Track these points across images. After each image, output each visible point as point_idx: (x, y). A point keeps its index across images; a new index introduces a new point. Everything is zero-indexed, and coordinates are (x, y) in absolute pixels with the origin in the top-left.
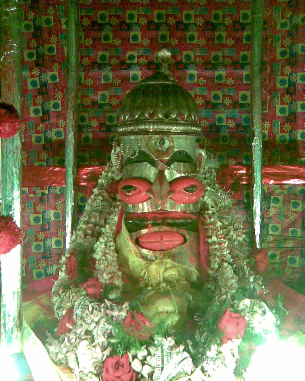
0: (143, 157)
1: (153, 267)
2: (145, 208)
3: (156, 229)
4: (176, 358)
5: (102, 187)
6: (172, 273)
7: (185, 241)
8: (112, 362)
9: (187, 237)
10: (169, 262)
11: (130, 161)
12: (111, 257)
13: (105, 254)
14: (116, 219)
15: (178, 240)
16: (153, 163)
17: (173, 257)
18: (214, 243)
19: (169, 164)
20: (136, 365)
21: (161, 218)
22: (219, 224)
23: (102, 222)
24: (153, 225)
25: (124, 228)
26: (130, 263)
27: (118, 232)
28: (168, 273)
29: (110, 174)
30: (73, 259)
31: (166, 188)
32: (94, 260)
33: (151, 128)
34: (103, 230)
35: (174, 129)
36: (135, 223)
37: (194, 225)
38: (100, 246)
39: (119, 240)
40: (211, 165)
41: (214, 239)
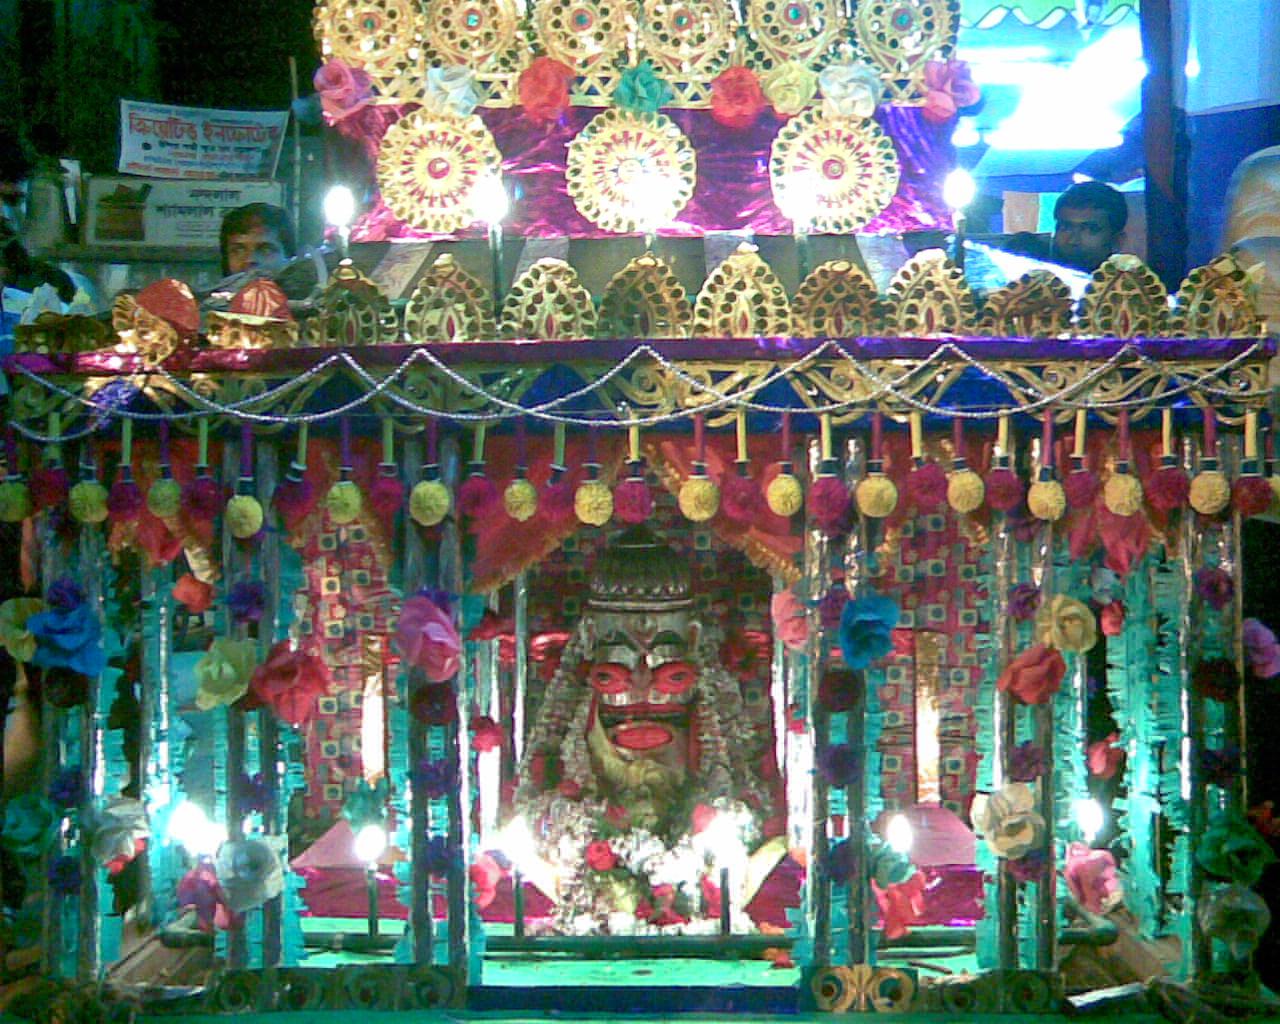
0: (621, 640)
1: (633, 768)
2: (622, 699)
3: (635, 725)
4: (650, 843)
5: (566, 667)
6: (655, 775)
7: (671, 739)
8: (594, 846)
9: (674, 733)
10: (651, 763)
11: (602, 643)
12: (583, 757)
13: (575, 755)
14: (586, 710)
15: (662, 738)
16: (633, 648)
17: (657, 758)
18: (706, 742)
19: (651, 648)
20: (615, 850)
21: (641, 711)
22: (717, 718)
23: (569, 715)
24: (634, 719)
25: (598, 724)
26: (606, 765)
27: (589, 727)
28: (650, 775)
29: (577, 650)
30: (1218, 795)
31: (648, 676)
32: (562, 764)
33: (630, 605)
34: (570, 725)
35: (658, 606)
36: (612, 718)
37: (686, 718)
38: (568, 746)
39: (592, 738)
40: (713, 636)
41: (707, 737)
